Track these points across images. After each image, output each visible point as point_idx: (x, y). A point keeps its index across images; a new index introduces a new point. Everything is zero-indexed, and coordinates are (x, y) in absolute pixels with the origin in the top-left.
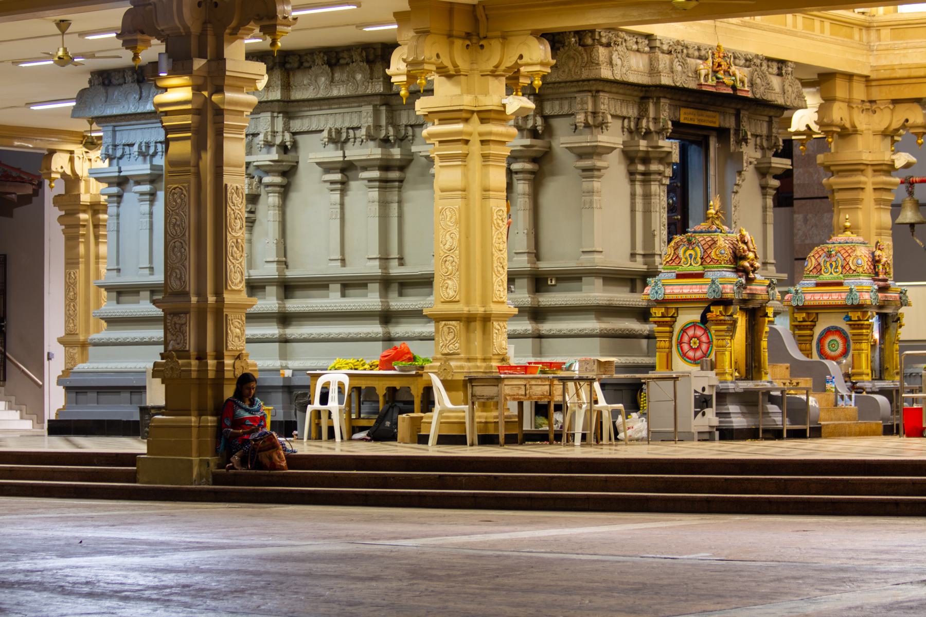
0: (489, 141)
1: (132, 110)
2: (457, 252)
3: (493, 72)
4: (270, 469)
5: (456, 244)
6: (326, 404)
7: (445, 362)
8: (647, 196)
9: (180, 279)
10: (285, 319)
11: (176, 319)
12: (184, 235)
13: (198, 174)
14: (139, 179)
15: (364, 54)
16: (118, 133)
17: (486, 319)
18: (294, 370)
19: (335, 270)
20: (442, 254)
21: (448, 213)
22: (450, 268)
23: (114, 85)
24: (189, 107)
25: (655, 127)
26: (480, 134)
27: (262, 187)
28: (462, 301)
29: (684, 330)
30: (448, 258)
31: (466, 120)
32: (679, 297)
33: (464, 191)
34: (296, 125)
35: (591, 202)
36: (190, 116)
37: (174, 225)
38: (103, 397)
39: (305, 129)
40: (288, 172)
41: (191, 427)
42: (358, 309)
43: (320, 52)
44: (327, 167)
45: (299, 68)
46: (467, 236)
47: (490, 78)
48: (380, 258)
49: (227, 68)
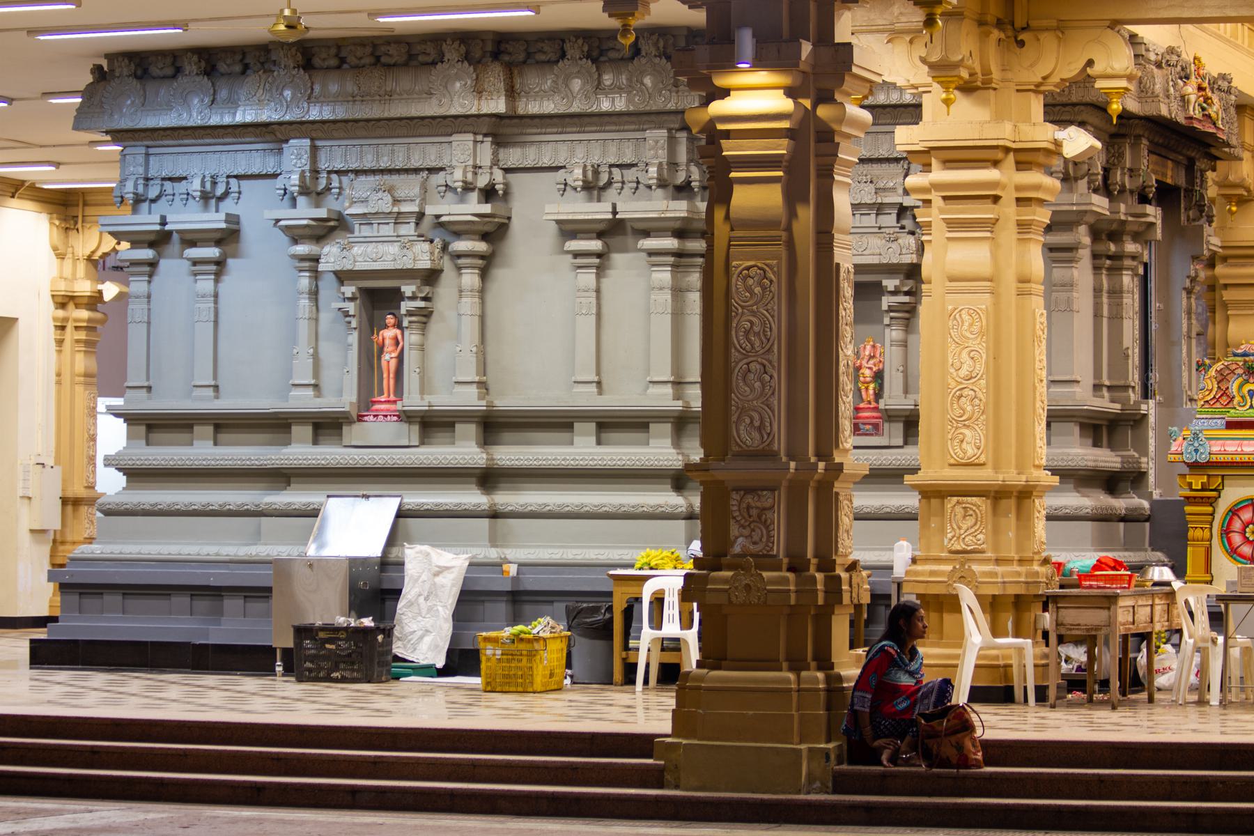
0: (1029, 199)
1: (196, 120)
2: (983, 382)
3: (1038, 85)
4: (958, 767)
5: (980, 368)
6: (660, 628)
7: (962, 565)
8: (1116, 293)
9: (760, 429)
10: (488, 478)
11: (749, 499)
12: (769, 350)
13: (790, 244)
14: (188, 237)
15: (661, 44)
16: (151, 158)
17: (1024, 495)
18: (520, 565)
19: (586, 399)
20: (953, 384)
21: (965, 317)
22: (969, 408)
23: (154, 78)
24: (785, 124)
25: (1130, 182)
26: (1018, 188)
27: (446, 258)
28: (990, 464)
29: (1234, 512)
30: (965, 392)
31: (996, 163)
32: (1237, 458)
33: (991, 280)
34: (513, 156)
35: (1069, 302)
36: (785, 142)
37: (747, 333)
38: (133, 603)
39: (529, 163)
40: (495, 232)
41: (790, 690)
42: (638, 465)
43: (577, 37)
44: (569, 230)
45: (406, 64)
46: (996, 357)
47: (1032, 95)
48: (673, 383)
49: (855, 61)
